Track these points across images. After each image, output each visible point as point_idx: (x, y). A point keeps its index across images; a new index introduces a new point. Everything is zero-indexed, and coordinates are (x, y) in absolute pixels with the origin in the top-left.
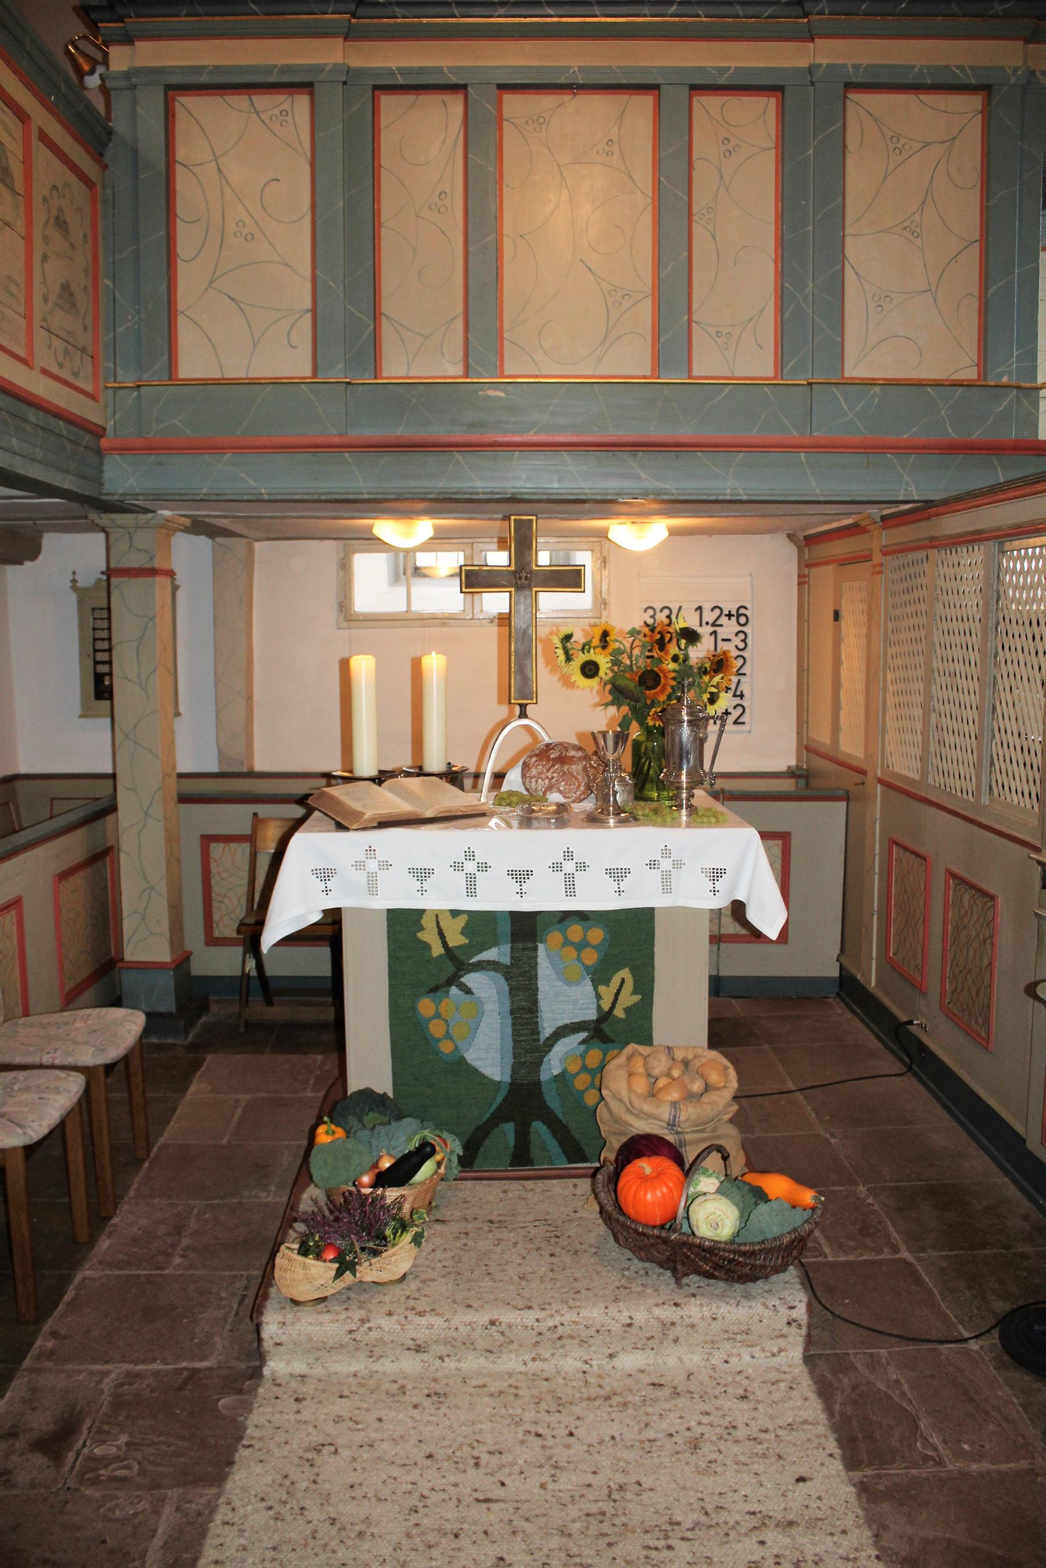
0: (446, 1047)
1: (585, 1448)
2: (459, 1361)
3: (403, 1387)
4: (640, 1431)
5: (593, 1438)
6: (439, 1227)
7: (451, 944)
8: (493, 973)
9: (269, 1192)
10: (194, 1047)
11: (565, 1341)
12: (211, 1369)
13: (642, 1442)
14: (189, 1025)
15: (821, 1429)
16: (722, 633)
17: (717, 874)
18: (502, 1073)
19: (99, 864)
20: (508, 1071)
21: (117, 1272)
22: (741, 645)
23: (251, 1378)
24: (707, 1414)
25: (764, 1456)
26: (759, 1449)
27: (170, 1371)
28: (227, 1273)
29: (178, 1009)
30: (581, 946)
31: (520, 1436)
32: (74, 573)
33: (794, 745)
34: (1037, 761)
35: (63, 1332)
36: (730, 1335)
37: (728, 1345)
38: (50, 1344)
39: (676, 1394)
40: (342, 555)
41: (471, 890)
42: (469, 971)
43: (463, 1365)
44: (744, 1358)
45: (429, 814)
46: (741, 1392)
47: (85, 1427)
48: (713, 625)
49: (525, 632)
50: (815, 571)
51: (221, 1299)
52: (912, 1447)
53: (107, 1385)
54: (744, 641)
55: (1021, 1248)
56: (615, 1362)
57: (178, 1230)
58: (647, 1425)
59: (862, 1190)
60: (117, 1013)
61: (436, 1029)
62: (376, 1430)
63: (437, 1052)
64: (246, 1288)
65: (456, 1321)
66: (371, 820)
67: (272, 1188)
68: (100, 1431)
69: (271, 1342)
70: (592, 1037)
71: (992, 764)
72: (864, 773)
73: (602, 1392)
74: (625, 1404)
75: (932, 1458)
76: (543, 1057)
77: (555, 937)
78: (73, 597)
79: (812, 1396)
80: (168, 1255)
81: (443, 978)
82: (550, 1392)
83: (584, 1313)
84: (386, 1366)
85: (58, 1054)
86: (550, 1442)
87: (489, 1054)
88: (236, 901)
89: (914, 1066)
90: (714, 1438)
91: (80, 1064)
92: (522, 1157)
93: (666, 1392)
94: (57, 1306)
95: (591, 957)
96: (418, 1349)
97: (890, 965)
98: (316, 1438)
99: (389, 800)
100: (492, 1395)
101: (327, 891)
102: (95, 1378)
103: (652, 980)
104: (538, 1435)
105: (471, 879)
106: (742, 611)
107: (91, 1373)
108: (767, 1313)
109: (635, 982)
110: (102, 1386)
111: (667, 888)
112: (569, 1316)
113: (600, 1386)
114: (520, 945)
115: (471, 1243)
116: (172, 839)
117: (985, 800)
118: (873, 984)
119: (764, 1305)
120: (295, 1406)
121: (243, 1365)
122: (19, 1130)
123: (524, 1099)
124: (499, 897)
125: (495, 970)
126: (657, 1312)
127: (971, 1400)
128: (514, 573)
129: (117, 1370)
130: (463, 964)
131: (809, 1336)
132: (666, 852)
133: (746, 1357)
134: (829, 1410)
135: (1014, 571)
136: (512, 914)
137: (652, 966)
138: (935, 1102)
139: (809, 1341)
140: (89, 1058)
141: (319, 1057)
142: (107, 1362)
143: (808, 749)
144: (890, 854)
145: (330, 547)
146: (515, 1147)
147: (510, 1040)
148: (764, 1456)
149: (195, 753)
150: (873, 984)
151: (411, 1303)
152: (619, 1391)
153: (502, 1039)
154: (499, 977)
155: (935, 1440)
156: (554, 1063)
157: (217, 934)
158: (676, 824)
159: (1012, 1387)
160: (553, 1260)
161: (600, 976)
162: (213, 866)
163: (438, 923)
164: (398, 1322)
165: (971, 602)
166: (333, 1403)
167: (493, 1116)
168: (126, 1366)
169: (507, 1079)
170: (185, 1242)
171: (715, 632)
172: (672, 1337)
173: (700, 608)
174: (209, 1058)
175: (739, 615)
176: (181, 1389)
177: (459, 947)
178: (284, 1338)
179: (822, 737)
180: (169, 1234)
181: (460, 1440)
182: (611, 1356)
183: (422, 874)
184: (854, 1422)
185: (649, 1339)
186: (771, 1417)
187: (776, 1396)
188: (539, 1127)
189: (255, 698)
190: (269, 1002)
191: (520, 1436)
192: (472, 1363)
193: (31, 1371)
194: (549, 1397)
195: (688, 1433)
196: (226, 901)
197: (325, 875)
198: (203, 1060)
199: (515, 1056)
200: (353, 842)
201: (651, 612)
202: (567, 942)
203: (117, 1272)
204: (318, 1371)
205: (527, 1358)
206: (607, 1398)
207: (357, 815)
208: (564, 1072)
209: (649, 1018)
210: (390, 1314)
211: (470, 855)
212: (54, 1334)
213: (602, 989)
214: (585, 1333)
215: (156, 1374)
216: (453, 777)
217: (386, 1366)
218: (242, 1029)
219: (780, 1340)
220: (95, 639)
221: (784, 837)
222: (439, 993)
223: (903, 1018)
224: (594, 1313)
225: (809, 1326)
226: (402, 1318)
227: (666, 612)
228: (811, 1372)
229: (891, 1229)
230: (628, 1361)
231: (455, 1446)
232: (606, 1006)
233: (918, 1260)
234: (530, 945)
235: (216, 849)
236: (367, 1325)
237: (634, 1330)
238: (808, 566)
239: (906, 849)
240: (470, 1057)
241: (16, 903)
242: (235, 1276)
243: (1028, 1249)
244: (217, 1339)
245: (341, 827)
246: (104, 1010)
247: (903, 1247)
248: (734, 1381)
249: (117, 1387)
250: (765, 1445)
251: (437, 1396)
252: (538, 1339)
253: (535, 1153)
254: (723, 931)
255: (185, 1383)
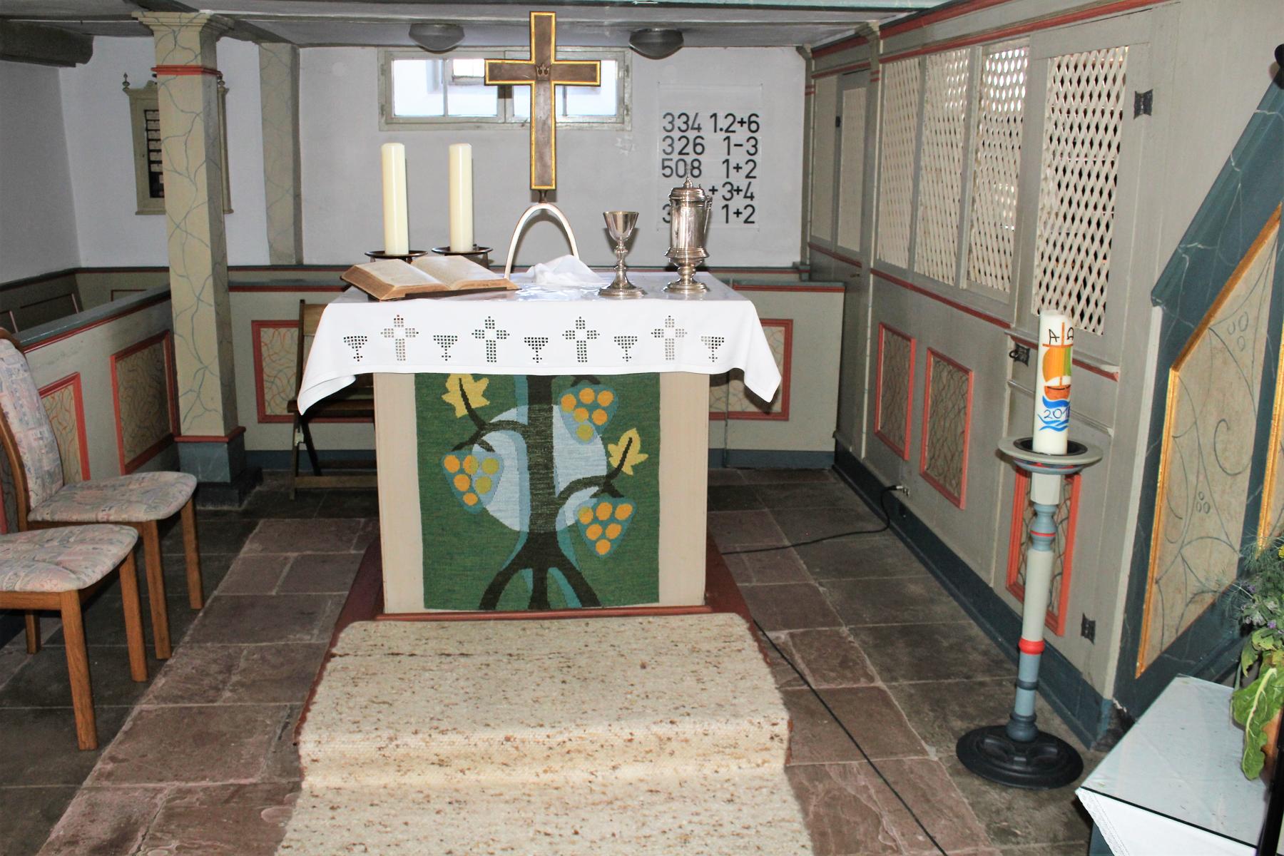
0: (470, 500)
1: (588, 844)
2: (478, 773)
3: (428, 796)
4: (638, 829)
5: (596, 837)
6: (463, 660)
7: (473, 406)
8: (512, 432)
9: (312, 635)
10: (246, 513)
11: (573, 755)
12: (255, 785)
13: (638, 838)
14: (243, 494)
15: (797, 826)
16: (735, 139)
17: (716, 342)
18: (521, 524)
19: (157, 346)
20: (527, 521)
21: (171, 705)
22: (753, 150)
23: (291, 791)
24: (697, 814)
25: (745, 848)
26: (741, 842)
27: (218, 787)
28: (273, 704)
29: (232, 479)
30: (593, 407)
31: (531, 834)
32: (126, 76)
33: (799, 245)
34: (1010, 247)
35: (121, 757)
36: (720, 749)
37: (718, 758)
38: (110, 767)
39: (671, 798)
40: (382, 62)
41: (491, 356)
42: (491, 430)
43: (482, 777)
44: (732, 769)
45: (453, 288)
46: (729, 796)
47: (140, 835)
48: (727, 131)
49: (544, 123)
50: (820, 81)
51: (267, 726)
52: (874, 839)
53: (160, 800)
54: (754, 146)
55: (980, 678)
56: (618, 773)
57: (229, 669)
58: (643, 824)
59: (844, 630)
60: (171, 476)
61: (460, 483)
62: (402, 832)
63: (461, 505)
64: (289, 716)
65: (474, 739)
66: (399, 292)
67: (316, 632)
68: (153, 838)
69: (308, 759)
70: (603, 491)
71: (970, 251)
72: (858, 264)
73: (605, 798)
74: (625, 808)
75: (891, 848)
76: (557, 510)
77: (568, 399)
78: (126, 99)
79: (791, 799)
80: (217, 689)
81: (466, 437)
82: (560, 799)
83: (591, 730)
84: (413, 779)
85: (113, 511)
86: (557, 839)
87: (509, 507)
88: (285, 381)
89: (893, 524)
90: (702, 834)
91: (134, 520)
92: (539, 602)
93: (662, 797)
94: (115, 735)
95: (601, 418)
96: (441, 763)
97: (878, 437)
98: (348, 838)
99: (416, 275)
100: (507, 802)
101: (358, 357)
102: (149, 794)
103: (659, 440)
104: (547, 834)
105: (491, 346)
106: (753, 118)
107: (146, 790)
108: (754, 729)
109: (642, 442)
110: (156, 801)
111: (670, 354)
112: (577, 733)
113: (604, 793)
114: (537, 407)
115: (491, 673)
116: (224, 325)
117: (964, 284)
118: (863, 455)
119: (751, 722)
120: (331, 814)
121: (284, 781)
122: (73, 576)
123: (541, 548)
124: (517, 362)
125: (514, 429)
126: (655, 729)
127: (928, 801)
128: (535, 66)
129: (169, 787)
130: (484, 424)
131: (789, 749)
132: (670, 321)
133: (734, 768)
134: (805, 811)
135: (995, 73)
136: (530, 378)
137: (658, 427)
138: (914, 558)
139: (790, 755)
140: (143, 514)
141: (363, 520)
142: (161, 780)
143: (811, 246)
144: (880, 337)
145: (371, 52)
146: (534, 591)
147: (528, 493)
148: (745, 848)
149: (249, 245)
150: (863, 455)
151: (435, 723)
152: (620, 796)
153: (521, 491)
154: (518, 436)
155: (895, 833)
156: (568, 515)
157: (268, 412)
158: (682, 298)
159: (963, 790)
160: (564, 686)
161: (609, 435)
162: (264, 349)
163: (461, 386)
164: (423, 740)
165: (956, 105)
166: (365, 810)
167: (513, 563)
168: (177, 784)
169: (526, 529)
170: (235, 678)
171: (728, 138)
172: (668, 750)
173: (715, 115)
174: (261, 522)
175: (750, 123)
176: (227, 801)
177: (482, 408)
178: (320, 756)
179: (824, 234)
180: (221, 672)
181: (476, 838)
182: (614, 768)
183: (446, 341)
184: (826, 820)
185: (647, 752)
186: (754, 817)
187: (759, 799)
188: (555, 574)
189: (303, 197)
190: (318, 473)
191: (531, 834)
192: (490, 776)
193: (90, 789)
194: (557, 803)
195: (679, 831)
196: (277, 381)
197: (357, 341)
198: (256, 524)
199: (533, 508)
200: (383, 312)
201: (669, 118)
202: (580, 404)
203: (171, 705)
204: (352, 784)
205: (540, 770)
206: (611, 803)
207: (386, 288)
208: (577, 522)
209: (655, 476)
210: (416, 733)
211: (490, 324)
212: (113, 759)
213: (611, 447)
214: (590, 748)
215: (205, 789)
216: (478, 255)
217: (413, 779)
218: (292, 497)
219: (764, 753)
220: (149, 140)
221: (787, 324)
222: (463, 451)
223: (887, 483)
224: (598, 730)
225: (790, 740)
226: (426, 736)
227: (684, 118)
228: (790, 780)
229: (868, 662)
230: (630, 772)
231: (472, 844)
232: (615, 464)
233: (890, 688)
234: (546, 407)
235: (267, 334)
236: (395, 743)
237: (635, 744)
238: (816, 77)
239: (894, 332)
240: (492, 509)
241: (74, 379)
242: (278, 707)
243: (987, 679)
244: (261, 759)
245: (372, 299)
246: (157, 474)
247: (877, 677)
248: (722, 788)
249: (169, 801)
250: (746, 839)
251: (457, 803)
252: (549, 753)
253: (551, 596)
254: (731, 409)
255: (232, 796)
